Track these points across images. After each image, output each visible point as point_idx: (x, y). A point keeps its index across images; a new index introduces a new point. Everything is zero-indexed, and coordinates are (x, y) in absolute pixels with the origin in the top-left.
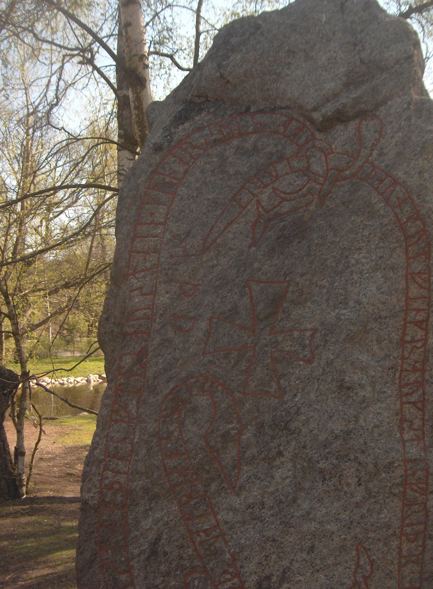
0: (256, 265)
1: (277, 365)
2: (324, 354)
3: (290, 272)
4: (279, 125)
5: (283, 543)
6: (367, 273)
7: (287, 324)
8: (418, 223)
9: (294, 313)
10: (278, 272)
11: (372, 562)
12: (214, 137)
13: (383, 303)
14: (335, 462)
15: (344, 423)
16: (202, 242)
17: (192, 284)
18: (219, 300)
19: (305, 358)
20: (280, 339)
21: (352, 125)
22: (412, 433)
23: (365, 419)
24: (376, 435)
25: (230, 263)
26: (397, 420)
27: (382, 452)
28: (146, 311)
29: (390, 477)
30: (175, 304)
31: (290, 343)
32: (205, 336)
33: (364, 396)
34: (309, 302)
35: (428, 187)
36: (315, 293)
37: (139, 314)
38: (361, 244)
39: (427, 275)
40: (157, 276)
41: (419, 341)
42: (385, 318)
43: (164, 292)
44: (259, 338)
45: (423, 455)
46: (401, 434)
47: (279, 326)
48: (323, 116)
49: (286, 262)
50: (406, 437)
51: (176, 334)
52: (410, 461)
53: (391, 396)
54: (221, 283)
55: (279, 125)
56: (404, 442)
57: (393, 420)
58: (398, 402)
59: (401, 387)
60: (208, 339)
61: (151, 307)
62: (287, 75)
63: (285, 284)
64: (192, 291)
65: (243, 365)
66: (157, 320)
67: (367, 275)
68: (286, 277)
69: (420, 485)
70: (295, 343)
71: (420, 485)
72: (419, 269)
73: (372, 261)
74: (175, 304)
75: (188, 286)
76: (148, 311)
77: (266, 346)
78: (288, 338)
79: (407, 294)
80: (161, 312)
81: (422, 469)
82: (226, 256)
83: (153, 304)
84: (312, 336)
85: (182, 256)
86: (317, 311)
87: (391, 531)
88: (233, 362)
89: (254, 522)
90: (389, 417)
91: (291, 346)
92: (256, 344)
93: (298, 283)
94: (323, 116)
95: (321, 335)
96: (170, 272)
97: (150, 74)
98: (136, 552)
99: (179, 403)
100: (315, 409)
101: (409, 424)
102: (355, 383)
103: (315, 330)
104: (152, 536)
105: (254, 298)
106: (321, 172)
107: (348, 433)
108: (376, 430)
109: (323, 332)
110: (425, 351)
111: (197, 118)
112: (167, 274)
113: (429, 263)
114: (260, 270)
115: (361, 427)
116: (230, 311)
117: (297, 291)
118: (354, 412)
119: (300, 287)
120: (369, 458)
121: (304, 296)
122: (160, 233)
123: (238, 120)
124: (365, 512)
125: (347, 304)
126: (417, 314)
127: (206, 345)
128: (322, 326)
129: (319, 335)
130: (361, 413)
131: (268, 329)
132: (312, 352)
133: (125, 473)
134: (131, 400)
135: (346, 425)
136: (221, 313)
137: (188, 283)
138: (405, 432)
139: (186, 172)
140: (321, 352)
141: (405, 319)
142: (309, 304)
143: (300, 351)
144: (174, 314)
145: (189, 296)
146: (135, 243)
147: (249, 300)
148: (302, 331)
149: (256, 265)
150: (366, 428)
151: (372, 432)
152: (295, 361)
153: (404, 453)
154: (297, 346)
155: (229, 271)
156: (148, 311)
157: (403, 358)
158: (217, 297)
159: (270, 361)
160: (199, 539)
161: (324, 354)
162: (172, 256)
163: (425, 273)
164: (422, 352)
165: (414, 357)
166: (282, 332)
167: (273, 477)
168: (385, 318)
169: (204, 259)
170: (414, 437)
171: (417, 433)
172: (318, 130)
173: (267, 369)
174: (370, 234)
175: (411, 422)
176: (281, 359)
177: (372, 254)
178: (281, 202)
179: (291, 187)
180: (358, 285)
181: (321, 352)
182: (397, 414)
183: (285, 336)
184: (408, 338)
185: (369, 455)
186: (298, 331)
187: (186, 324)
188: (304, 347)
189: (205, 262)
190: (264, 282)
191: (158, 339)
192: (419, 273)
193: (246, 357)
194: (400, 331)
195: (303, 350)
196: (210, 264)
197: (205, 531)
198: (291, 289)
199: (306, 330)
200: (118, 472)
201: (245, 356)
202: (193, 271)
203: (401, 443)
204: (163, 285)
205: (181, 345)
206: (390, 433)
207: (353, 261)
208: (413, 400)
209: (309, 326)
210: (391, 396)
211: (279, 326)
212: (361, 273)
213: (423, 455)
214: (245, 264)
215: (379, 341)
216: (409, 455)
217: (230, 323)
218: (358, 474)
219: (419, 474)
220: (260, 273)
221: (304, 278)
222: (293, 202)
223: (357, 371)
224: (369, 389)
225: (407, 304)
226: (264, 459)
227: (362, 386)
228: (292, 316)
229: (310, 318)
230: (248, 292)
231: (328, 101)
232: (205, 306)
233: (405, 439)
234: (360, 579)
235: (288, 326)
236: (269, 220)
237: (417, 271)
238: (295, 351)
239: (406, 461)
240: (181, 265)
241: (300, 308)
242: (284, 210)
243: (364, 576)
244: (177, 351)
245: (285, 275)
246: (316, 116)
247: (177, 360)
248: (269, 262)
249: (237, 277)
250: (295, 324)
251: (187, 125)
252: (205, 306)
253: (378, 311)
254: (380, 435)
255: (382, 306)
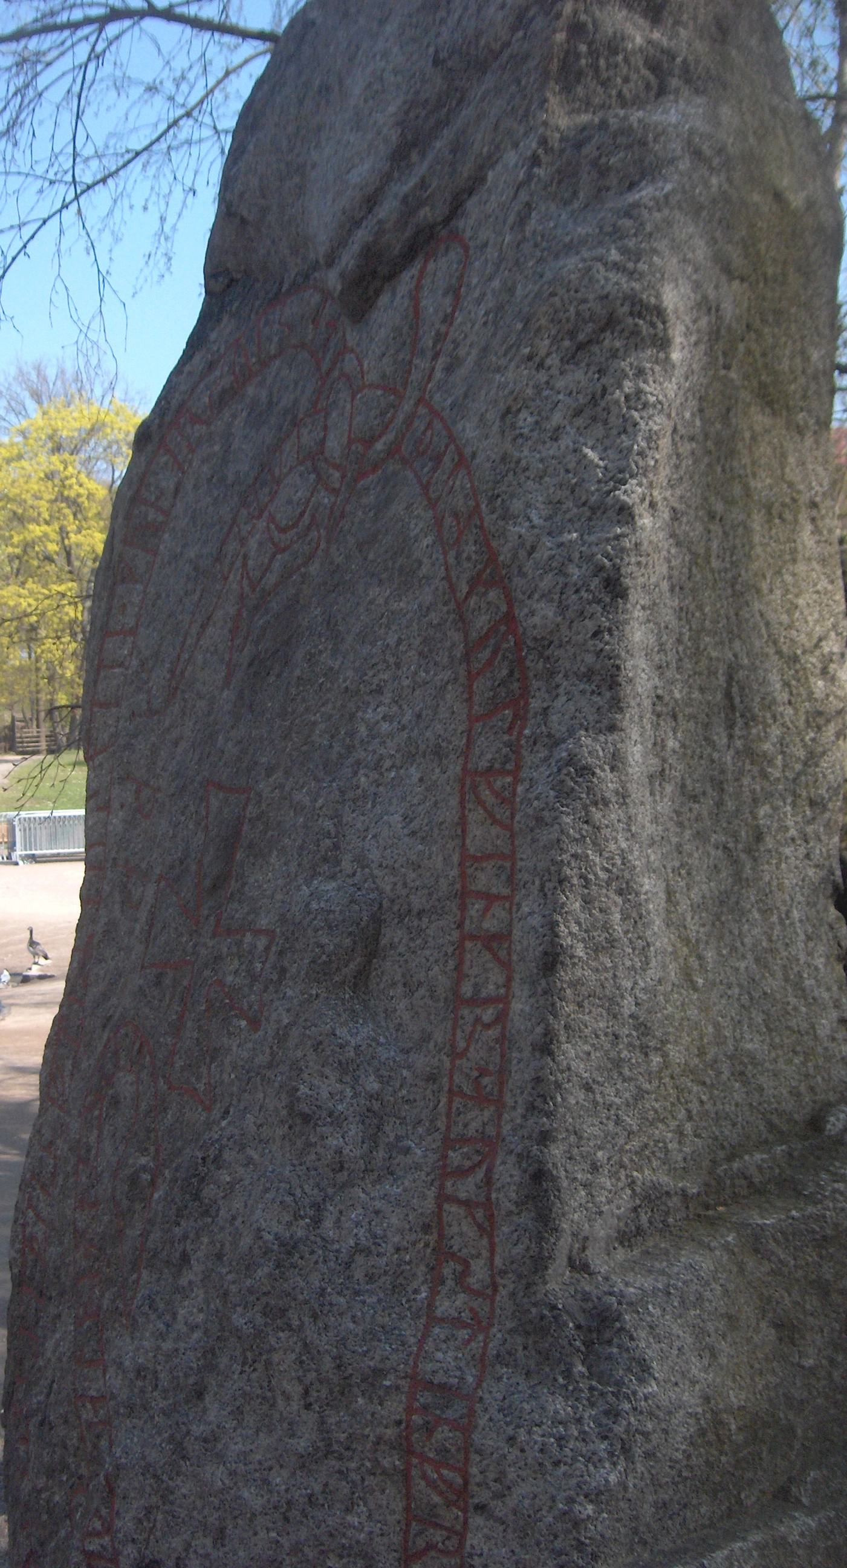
5: (172, 1493)
6: (392, 767)
14: (259, 1320)
15: (287, 1218)
22: (461, 1298)
23: (338, 1220)
24: (359, 1274)
26: (427, 1245)
27: (359, 1330)
29: (373, 1415)
33: (339, 1151)
35: (523, 463)
38: (381, 676)
39: (509, 779)
42: (420, 914)
45: (470, 1379)
46: (433, 1292)
50: (444, 1307)
52: (429, 1385)
53: (418, 1167)
56: (433, 1320)
57: (414, 1244)
58: (431, 1193)
59: (448, 1143)
67: (393, 774)
69: (445, 1472)
71: (445, 1472)
72: (489, 756)
73: (404, 728)
81: (454, 1425)
90: (401, 1231)
94: (342, 275)
100: (250, 1161)
101: (459, 1268)
102: (319, 1107)
107: (289, 1247)
108: (360, 1259)
110: (502, 1039)
113: (520, 733)
115: (323, 1239)
118: (316, 1191)
120: (324, 1338)
124: (318, 1488)
125: (338, 862)
126: (487, 909)
130: (331, 1199)
135: (289, 1224)
138: (444, 1290)
141: (460, 926)
150: (336, 1246)
151: (348, 1265)
153: (418, 1355)
163: (503, 772)
164: (497, 1041)
168: (420, 914)
170: (466, 1315)
171: (475, 1305)
174: (399, 642)
175: (466, 1264)
177: (405, 707)
180: (369, 806)
182: (426, 1228)
185: (326, 1328)
192: (490, 769)
203: (423, 1320)
206: (401, 1280)
207: (363, 730)
210: (418, 1167)
212: (377, 767)
213: (470, 1379)
215: (410, 989)
216: (429, 1367)
218: (300, 1373)
219: (443, 1433)
223: (327, 1071)
224: (354, 1130)
227: (337, 1120)
233: (439, 1313)
239: (418, 1382)
253: (404, 892)
254: (370, 1278)
255: (414, 875)
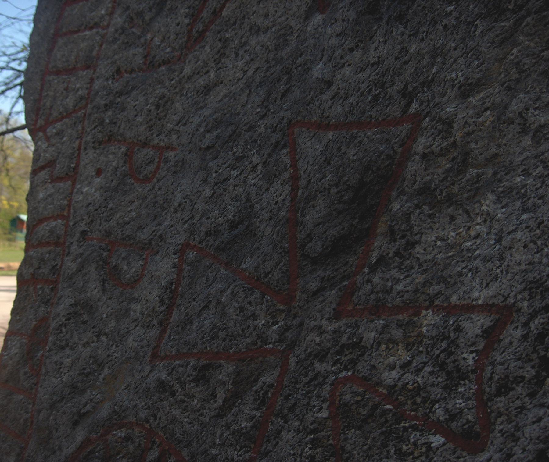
0: (318, 71)
1: (350, 433)
2: (531, 416)
3: (423, 84)
7: (398, 281)
9: (430, 238)
10: (383, 85)
16: (187, 21)
17: (154, 147)
18: (208, 192)
19: (454, 425)
20: (370, 336)
25: (250, 73)
28: (54, 223)
30: (110, 206)
31: (403, 355)
32: (162, 302)
34: (491, 197)
36: (518, 160)
40: (83, 128)
43: (91, 171)
44: (301, 324)
47: (368, 287)
49: (413, 49)
51: (104, 290)
54: (218, 137)
60: (170, 309)
61: (65, 214)
63: (404, 129)
64: (152, 168)
65: (246, 415)
66: (74, 248)
68: (409, 105)
70: (423, 358)
74: (110, 206)
75: (145, 151)
77: (322, 356)
78: (397, 334)
80: (83, 226)
82: (241, 53)
83: (69, 206)
84: (491, 335)
85: (140, 69)
86: (518, 235)
88: (221, 395)
91: (406, 366)
92: (292, 346)
93: (449, 123)
95: (525, 337)
96: (108, 116)
97: (488, 445)
103: (502, 313)
105: (303, 182)
109: (536, 324)
112: (101, 122)
114: (329, 84)
116: (233, 225)
117: (443, 153)
119: (458, 135)
121: (472, 172)
122: (103, 16)
127: (164, 331)
128: (531, 297)
129: (519, 333)
131: (332, 294)
132: (482, 402)
136: (208, 234)
137: (145, 144)
140: (522, 408)
142: (488, 204)
143: (437, 392)
144: (108, 233)
145: (146, 180)
147: (287, 189)
148: (451, 310)
149: (318, 71)
152: (414, 428)
154: (428, 369)
155: (244, 98)
158: (205, 181)
159: (325, 414)
161: (531, 416)
162: (118, 71)
166: (377, 309)
169: (187, 70)
173: (315, 443)
176: (364, 412)
181: (522, 408)
183: (386, 326)
186: (437, 310)
187: (129, 264)
188: (455, 376)
189: (190, 78)
190: (337, 127)
191: (69, 301)
193: (259, 384)
195: (449, 388)
196: (201, 81)
198: (421, 144)
199: (470, 308)
201: (256, 381)
202: (158, 107)
204: (91, 152)
205: (112, 324)
209: (480, 295)
211: (368, 287)
214: (288, 72)
217: (228, 265)
220: (329, 94)
221: (474, 100)
228: (419, 249)
229: (486, 260)
230: (287, 161)
232: (176, 212)
235: (400, 287)
238: (419, 389)
240: (134, 93)
241: (452, 218)
244: (103, 338)
245: (408, 95)
247: (101, 365)
248: (357, 54)
249: (263, 117)
250: (427, 284)
252: (176, 212)
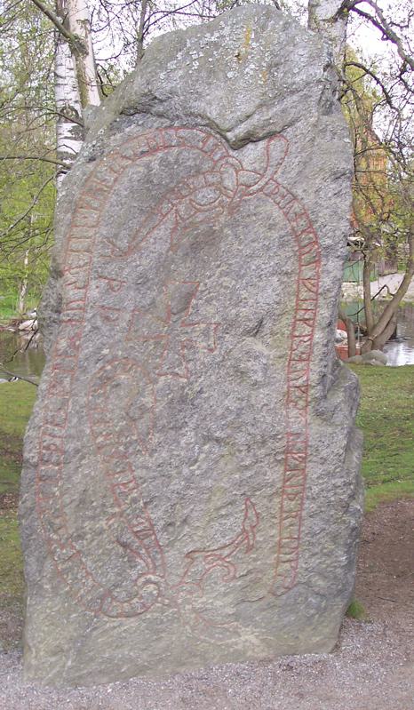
4: (198, 141)
8: (311, 235)
11: (257, 515)
12: (140, 150)
13: (277, 303)
21: (262, 144)
37: (74, 305)
41: (306, 336)
48: (236, 136)
55: (198, 141)
59: (289, 373)
62: (208, 95)
76: (81, 303)
79: (298, 296)
87: (274, 490)
89: (164, 478)
98: (68, 501)
99: (182, 98)
104: (81, 488)
106: (231, 187)
111: (128, 130)
123: (163, 133)
133: (59, 437)
134: (66, 377)
139: (116, 180)
146: (71, 243)
156: (81, 303)
157: (292, 349)
160: (118, 491)
165: (301, 349)
167: (179, 443)
172: (232, 148)
178: (195, 213)
179: (205, 200)
184: (297, 333)
194: (291, 328)
196: (134, 264)
197: (123, 484)
200: (54, 436)
208: (297, 384)
222: (207, 213)
225: (297, 304)
226: (172, 428)
231: (242, 122)
234: (248, 528)
236: (186, 228)
237: (307, 277)
242: (198, 220)
243: (251, 526)
246: (229, 135)
251: (118, 136)
